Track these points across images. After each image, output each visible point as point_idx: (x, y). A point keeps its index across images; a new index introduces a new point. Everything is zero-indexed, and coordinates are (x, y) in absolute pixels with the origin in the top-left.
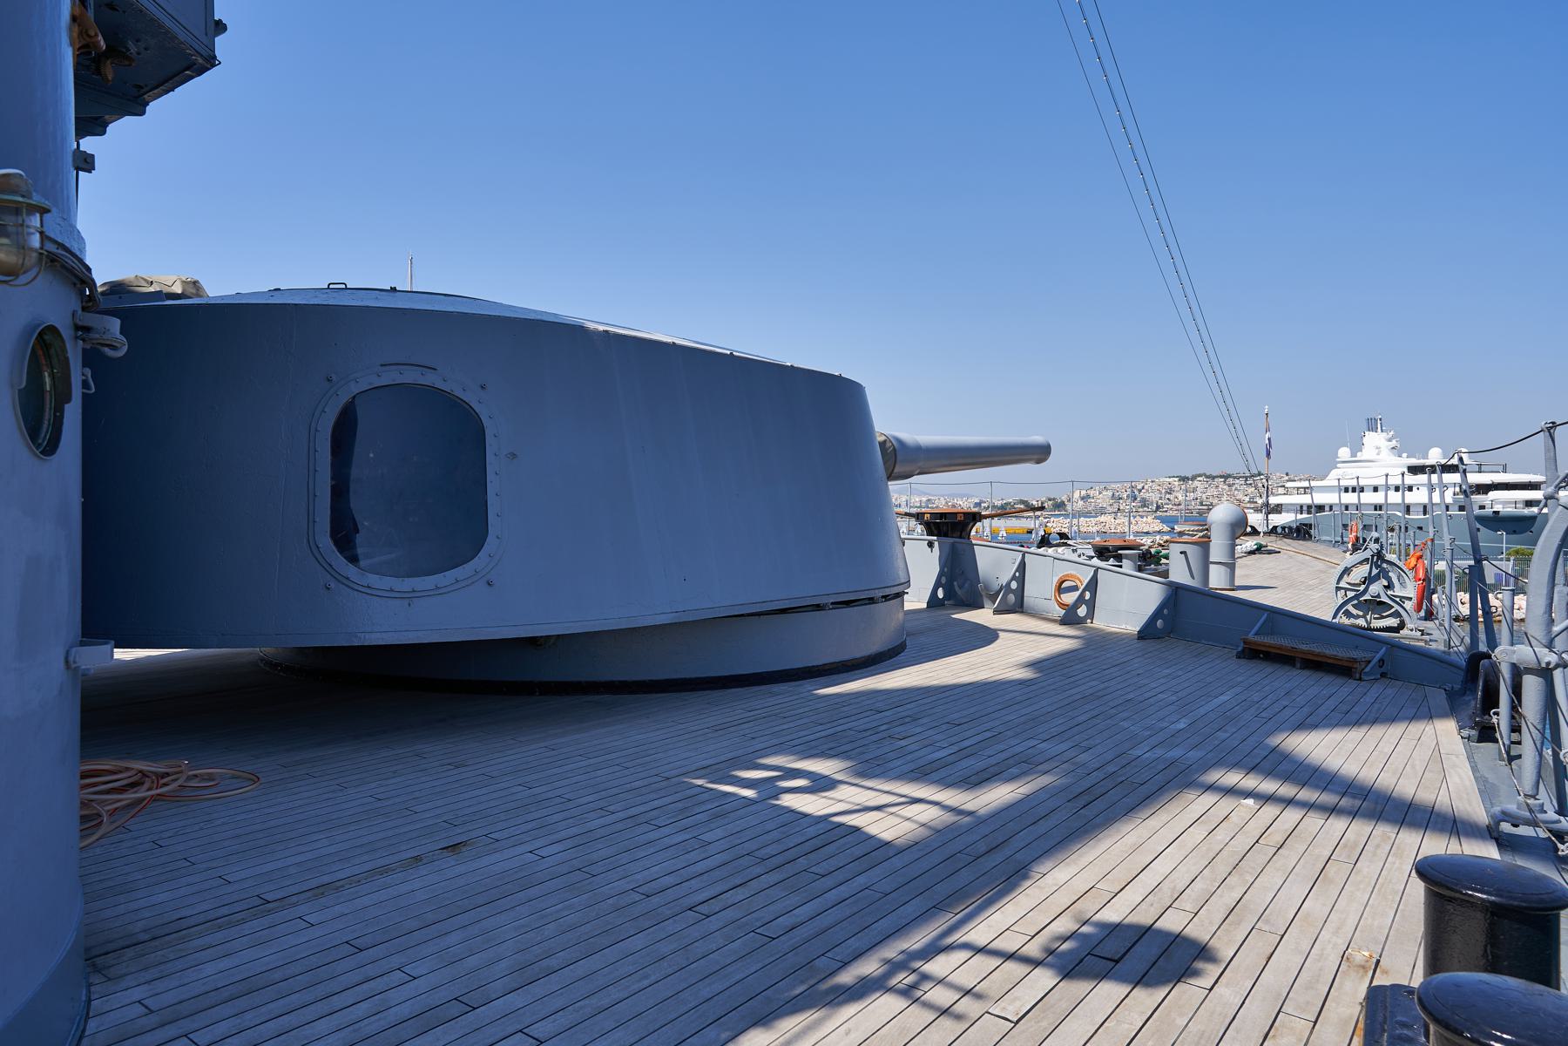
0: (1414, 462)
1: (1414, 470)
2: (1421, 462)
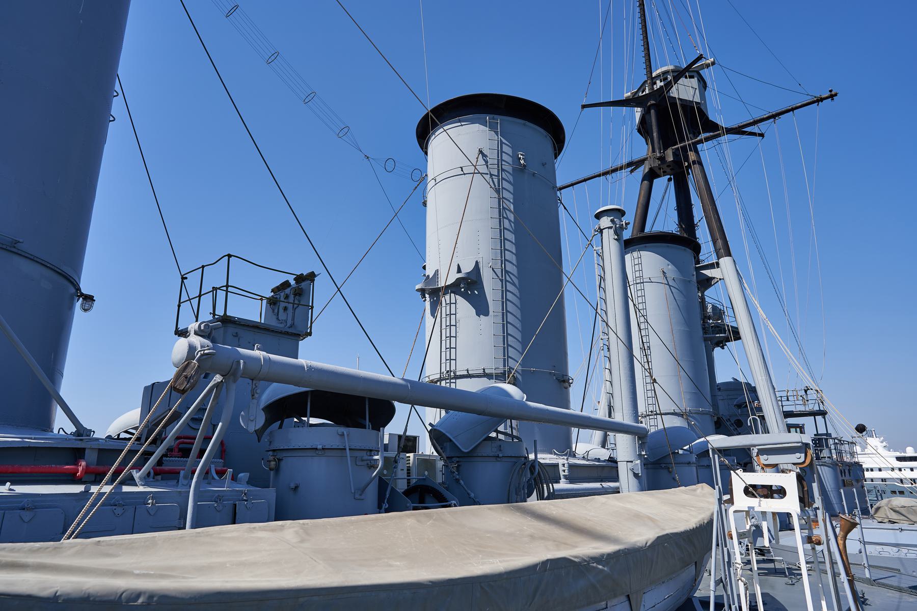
0: (898, 454)
1: (899, 459)
2: (903, 455)
